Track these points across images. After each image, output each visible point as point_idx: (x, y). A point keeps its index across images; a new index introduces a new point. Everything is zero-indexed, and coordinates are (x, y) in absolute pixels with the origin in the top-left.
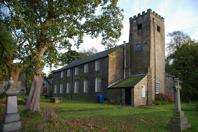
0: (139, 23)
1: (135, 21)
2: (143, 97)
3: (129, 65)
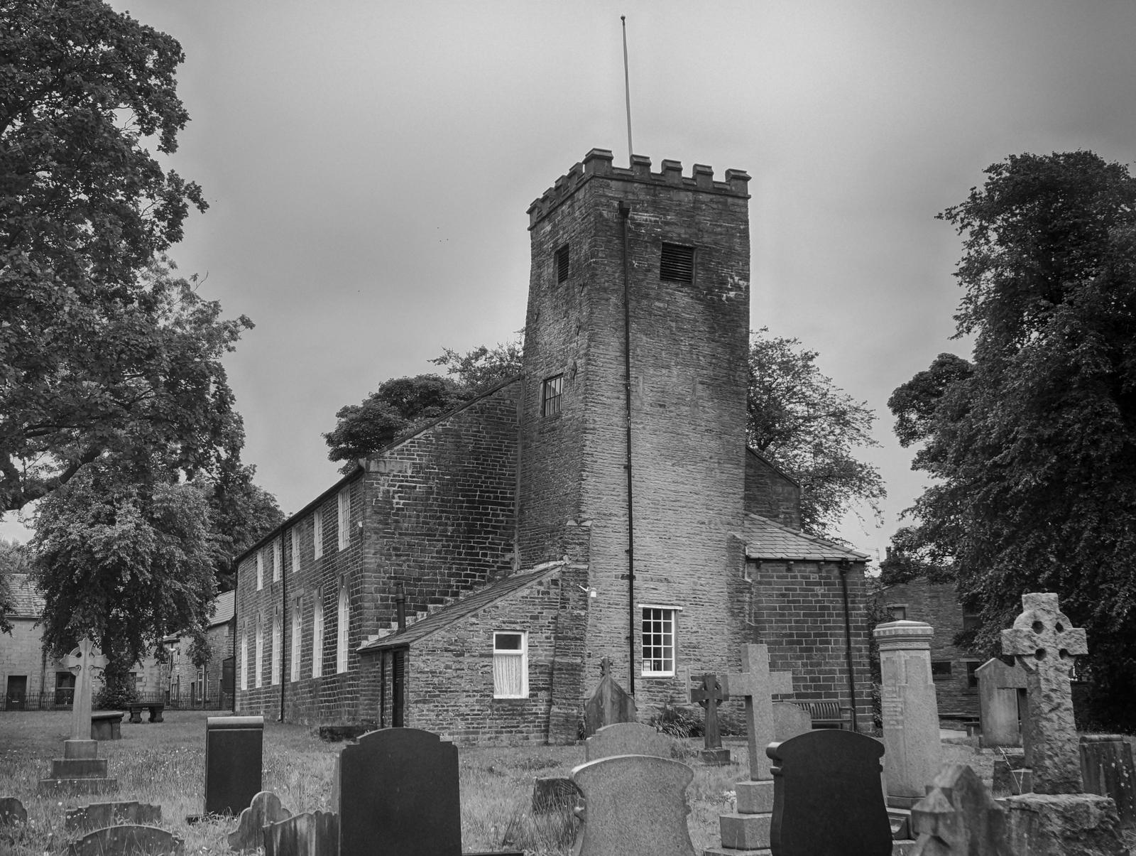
0: (563, 239)
1: (548, 228)
2: (500, 701)
3: (517, 508)
